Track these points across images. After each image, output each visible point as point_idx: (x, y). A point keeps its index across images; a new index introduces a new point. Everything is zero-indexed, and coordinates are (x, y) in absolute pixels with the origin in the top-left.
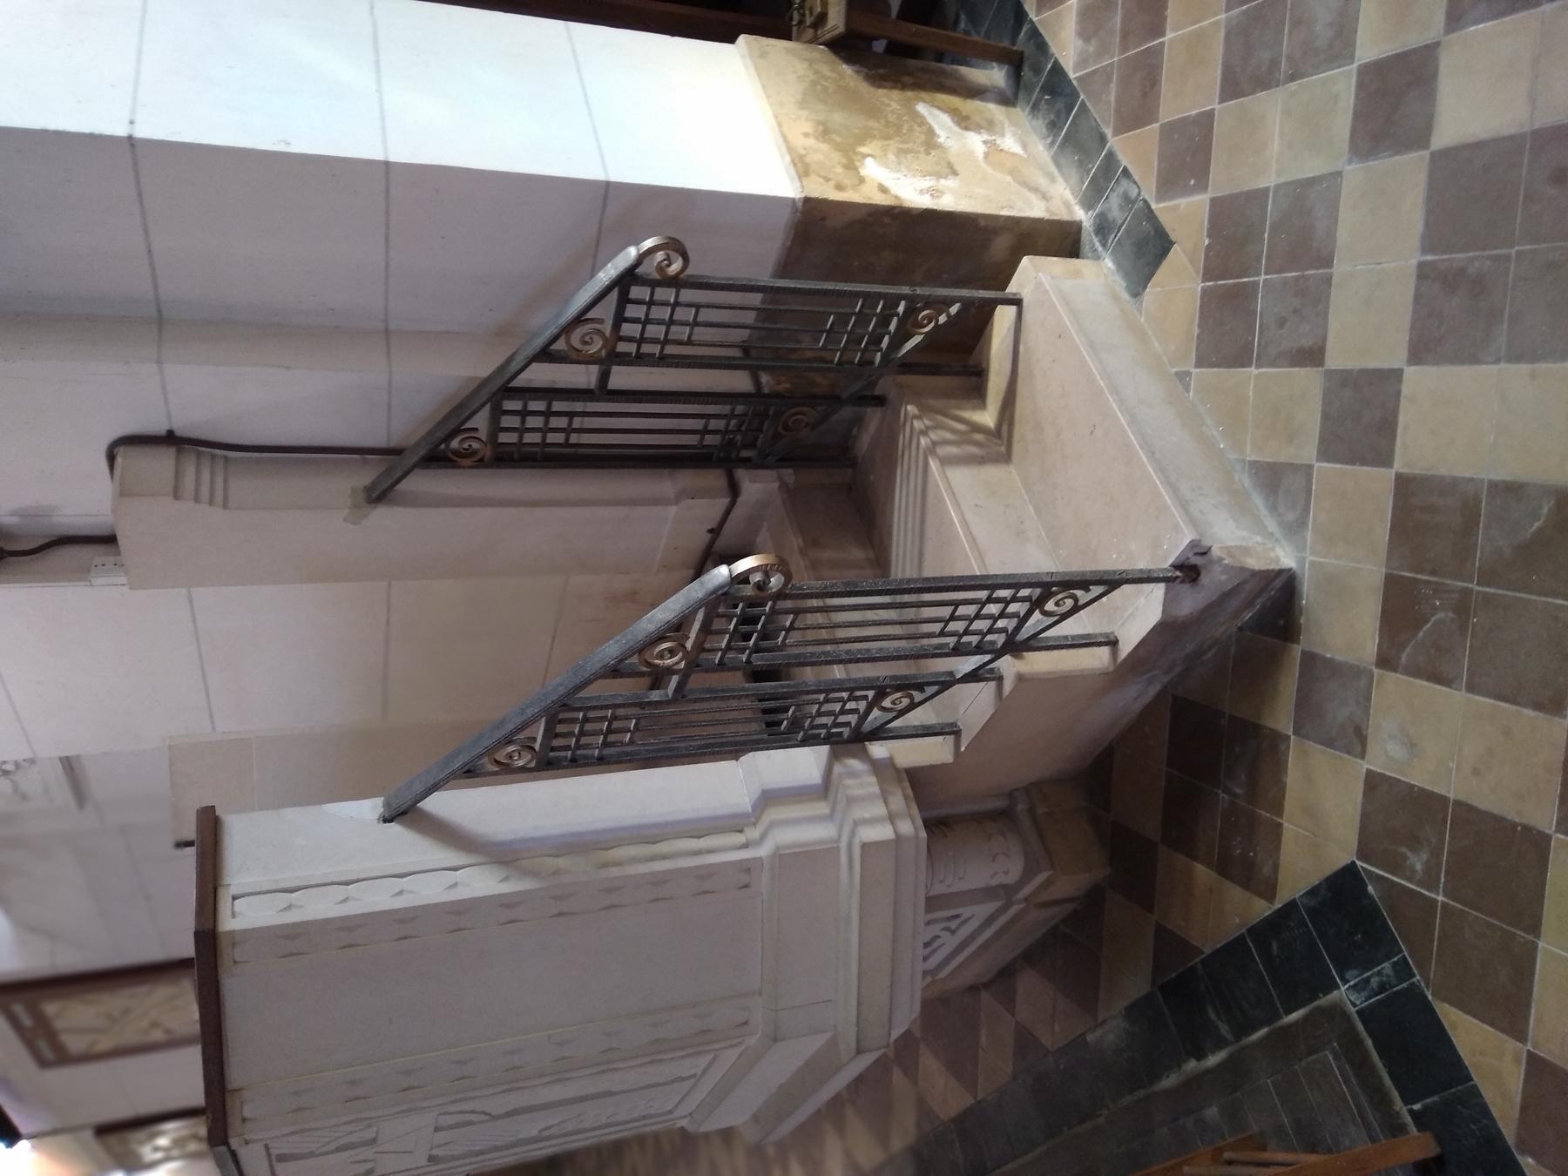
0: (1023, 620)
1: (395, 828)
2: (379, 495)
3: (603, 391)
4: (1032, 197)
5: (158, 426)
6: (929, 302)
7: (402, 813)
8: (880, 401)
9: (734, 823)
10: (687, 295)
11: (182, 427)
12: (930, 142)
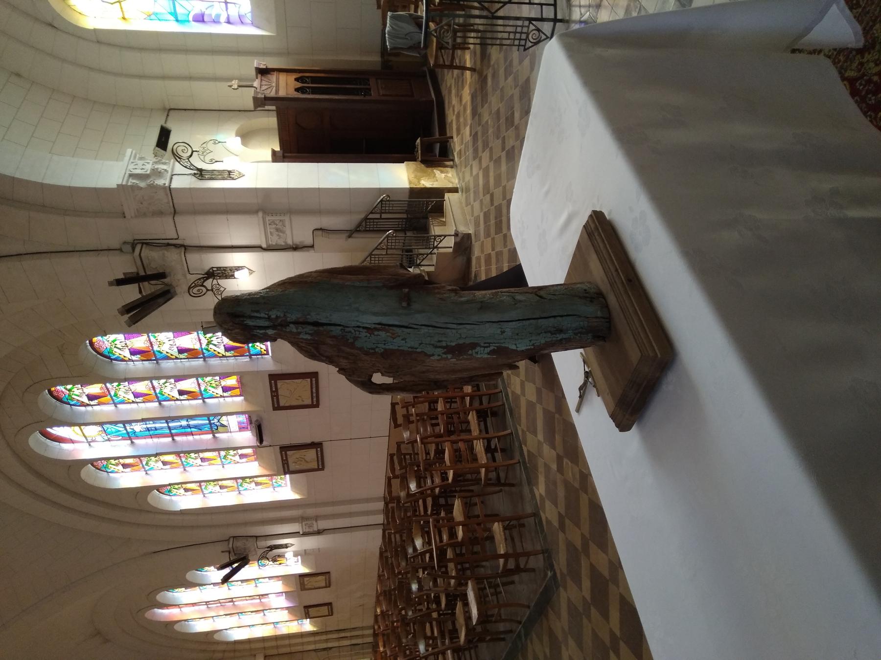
2: (350, 237)
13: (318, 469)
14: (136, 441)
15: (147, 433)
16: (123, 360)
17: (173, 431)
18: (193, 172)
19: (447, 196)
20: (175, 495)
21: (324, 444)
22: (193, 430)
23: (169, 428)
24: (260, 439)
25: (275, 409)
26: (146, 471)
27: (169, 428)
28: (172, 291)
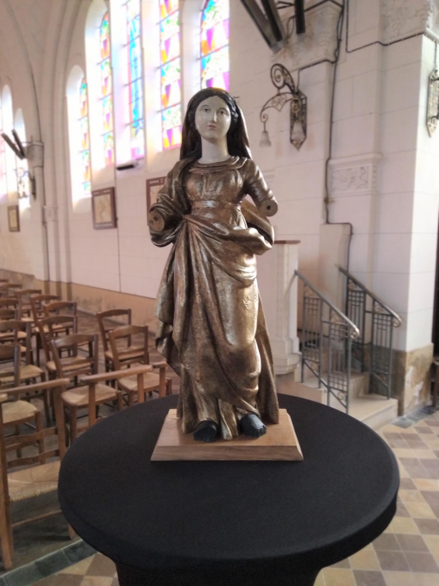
0: (337, 389)
3: (365, 311)
5: (354, 231)
6: (387, 380)
7: (296, 273)
9: (288, 335)
10: (389, 329)
11: (353, 236)
12: (417, 383)
14: (126, 49)
15: (133, 59)
16: (202, 22)
19: (394, 402)
20: (81, 93)
21: (114, 231)
23: (136, 81)
24: (121, 168)
25: (148, 181)
27: (136, 81)
28: (280, 44)
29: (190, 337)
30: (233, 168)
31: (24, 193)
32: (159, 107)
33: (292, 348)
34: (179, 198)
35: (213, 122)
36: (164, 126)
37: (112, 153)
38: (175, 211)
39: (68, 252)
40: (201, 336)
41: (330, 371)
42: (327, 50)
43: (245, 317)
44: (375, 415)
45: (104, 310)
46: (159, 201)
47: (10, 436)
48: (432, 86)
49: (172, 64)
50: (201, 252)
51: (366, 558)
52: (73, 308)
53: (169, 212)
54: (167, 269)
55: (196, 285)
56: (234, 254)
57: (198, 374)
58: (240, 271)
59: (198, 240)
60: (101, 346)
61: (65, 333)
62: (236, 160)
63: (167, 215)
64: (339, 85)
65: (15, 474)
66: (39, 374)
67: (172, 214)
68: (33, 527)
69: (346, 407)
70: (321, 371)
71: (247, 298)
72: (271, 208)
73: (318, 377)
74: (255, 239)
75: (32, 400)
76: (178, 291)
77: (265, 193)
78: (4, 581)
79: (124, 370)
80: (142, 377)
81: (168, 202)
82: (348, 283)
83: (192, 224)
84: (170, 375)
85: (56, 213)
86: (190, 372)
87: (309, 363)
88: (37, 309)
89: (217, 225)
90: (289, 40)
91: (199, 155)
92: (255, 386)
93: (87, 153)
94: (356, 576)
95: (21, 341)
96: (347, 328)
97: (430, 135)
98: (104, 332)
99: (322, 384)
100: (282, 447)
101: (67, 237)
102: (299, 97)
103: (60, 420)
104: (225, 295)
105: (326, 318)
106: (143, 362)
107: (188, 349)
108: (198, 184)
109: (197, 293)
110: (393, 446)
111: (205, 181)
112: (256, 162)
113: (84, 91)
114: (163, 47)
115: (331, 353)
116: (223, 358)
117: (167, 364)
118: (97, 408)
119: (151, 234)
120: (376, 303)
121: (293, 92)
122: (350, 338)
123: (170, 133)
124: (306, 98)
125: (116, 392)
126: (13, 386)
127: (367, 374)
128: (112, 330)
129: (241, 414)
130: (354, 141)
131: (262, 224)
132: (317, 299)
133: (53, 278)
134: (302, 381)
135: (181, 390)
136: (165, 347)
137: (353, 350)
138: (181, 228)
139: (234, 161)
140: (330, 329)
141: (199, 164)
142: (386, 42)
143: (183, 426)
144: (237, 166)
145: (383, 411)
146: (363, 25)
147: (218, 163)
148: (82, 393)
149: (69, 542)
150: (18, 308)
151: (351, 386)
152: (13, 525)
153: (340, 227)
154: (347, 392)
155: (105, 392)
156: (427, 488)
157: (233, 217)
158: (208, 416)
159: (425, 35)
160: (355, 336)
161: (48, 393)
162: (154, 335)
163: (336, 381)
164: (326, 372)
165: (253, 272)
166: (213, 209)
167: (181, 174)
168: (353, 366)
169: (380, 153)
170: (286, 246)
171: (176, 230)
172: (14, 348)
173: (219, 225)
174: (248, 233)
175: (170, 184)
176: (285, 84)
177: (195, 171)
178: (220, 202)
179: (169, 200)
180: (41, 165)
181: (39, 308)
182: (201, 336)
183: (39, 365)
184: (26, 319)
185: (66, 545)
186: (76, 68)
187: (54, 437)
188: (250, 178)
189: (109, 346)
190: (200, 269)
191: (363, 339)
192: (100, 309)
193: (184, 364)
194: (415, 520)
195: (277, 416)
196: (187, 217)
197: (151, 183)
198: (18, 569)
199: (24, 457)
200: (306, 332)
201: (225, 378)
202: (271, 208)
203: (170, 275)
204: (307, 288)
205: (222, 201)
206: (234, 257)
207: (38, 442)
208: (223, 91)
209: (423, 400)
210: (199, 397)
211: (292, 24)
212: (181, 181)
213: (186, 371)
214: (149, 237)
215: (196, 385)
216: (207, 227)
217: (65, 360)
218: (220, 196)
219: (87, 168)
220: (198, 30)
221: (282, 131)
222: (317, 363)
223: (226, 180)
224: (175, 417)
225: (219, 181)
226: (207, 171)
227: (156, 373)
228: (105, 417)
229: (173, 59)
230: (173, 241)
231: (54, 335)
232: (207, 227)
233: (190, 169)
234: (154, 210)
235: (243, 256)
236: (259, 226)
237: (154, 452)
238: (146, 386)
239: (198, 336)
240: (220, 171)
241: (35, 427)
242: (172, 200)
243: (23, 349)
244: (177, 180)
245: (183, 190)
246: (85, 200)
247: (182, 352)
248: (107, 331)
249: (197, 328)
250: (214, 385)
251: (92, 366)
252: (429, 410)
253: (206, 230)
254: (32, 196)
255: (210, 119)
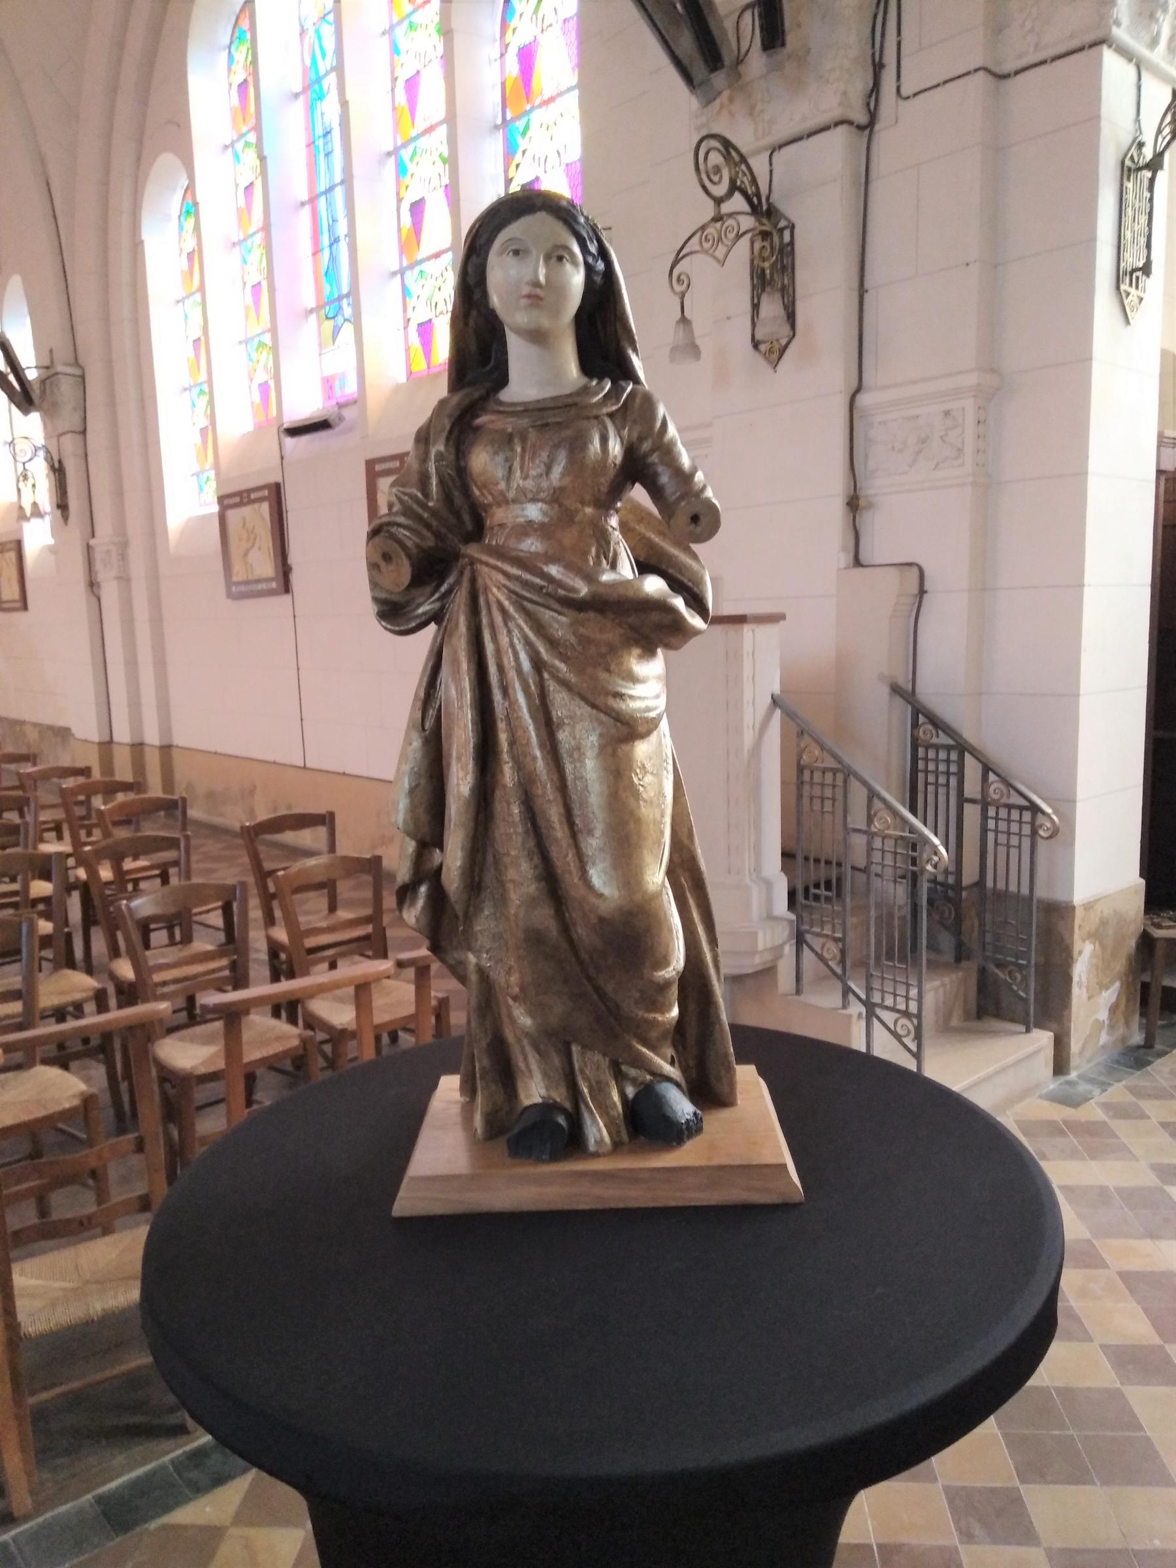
0: (893, 1009)
1: (769, 700)
2: (896, 690)
3: (962, 800)
4: (1080, 1045)
5: (927, 587)
6: (1025, 979)
7: (775, 702)
8: (958, 959)
9: (758, 869)
10: (1026, 843)
12: (1104, 987)
13: (229, 582)
15: (319, 131)
17: (322, 200)
18: (1148, 137)
19: (1043, 1038)
20: (181, 228)
22: (326, 254)
23: (331, 189)
24: (295, 431)
25: (370, 464)
26: (232, 144)
27: (331, 189)
28: (719, 79)
29: (489, 877)
30: (595, 412)
31: (35, 504)
32: (393, 261)
33: (769, 902)
34: (447, 498)
35: (536, 284)
36: (410, 314)
37: (270, 391)
38: (437, 535)
39: (161, 664)
40: (519, 876)
41: (872, 962)
42: (845, 93)
43: (638, 821)
44: (993, 1072)
45: (263, 815)
46: (395, 509)
47: (19, 1161)
48: (1129, 185)
49: (423, 142)
50: (512, 645)
51: (980, 1454)
52: (179, 813)
53: (423, 538)
54: (422, 694)
55: (503, 737)
56: (604, 650)
57: (514, 979)
58: (620, 696)
59: (503, 611)
60: (256, 914)
61: (158, 881)
62: (603, 389)
63: (418, 546)
64: (879, 189)
65: (31, 1264)
66: (91, 993)
67: (430, 542)
68: (82, 1404)
69: (917, 1056)
70: (848, 963)
71: (644, 767)
72: (702, 521)
73: (842, 978)
74: (661, 606)
75: (74, 1065)
76: (454, 754)
77: (685, 478)
78: (13, 1548)
79: (320, 975)
80: (369, 993)
81: (420, 511)
82: (915, 725)
83: (485, 569)
84: (442, 986)
85: (123, 557)
86: (493, 975)
87: (817, 943)
88: (82, 818)
89: (554, 570)
90: (742, 68)
91: (502, 380)
92: (670, 1009)
93: (202, 392)
94: (951, 1502)
95: (41, 907)
96: (915, 844)
97: (1128, 322)
98: (263, 875)
99: (851, 997)
100: (746, 1169)
101: (157, 621)
102: (775, 226)
103: (150, 1112)
104: (582, 762)
105: (857, 819)
106: (370, 953)
107: (486, 913)
108: (500, 459)
109: (505, 756)
110: (1044, 1157)
111: (519, 449)
112: (657, 395)
113: (190, 223)
114: (401, 97)
115: (873, 913)
116: (581, 931)
117: (434, 958)
118: (250, 1080)
119: (376, 600)
120: (992, 777)
121: (755, 210)
122: (923, 870)
123: (425, 330)
124: (792, 227)
125: (300, 1035)
126: (20, 1027)
127: (970, 968)
128: (284, 869)
129: (634, 1081)
130: (924, 345)
131: (680, 567)
132: (835, 771)
133: (123, 734)
134: (798, 992)
135: (469, 1022)
136: (423, 908)
137: (931, 902)
138: (458, 582)
139: (597, 393)
140: (870, 849)
141: (501, 403)
142: (1009, 67)
143: (478, 1121)
144: (606, 405)
145: (1016, 1064)
146: (940, 33)
147: (554, 399)
148: (207, 1040)
149: (185, 1438)
150: (29, 818)
151: (929, 1000)
152: (31, 1400)
153: (893, 574)
154: (919, 1016)
155: (268, 1036)
156: (1134, 1265)
157: (599, 546)
158: (543, 1092)
159: (1110, 46)
160: (935, 866)
161: (117, 1044)
162: (392, 876)
163: (889, 988)
164: (863, 963)
165: (657, 697)
166: (542, 525)
167: (451, 432)
168: (932, 947)
169: (994, 371)
170: (747, 630)
171: (443, 589)
172: (20, 924)
173: (561, 569)
174: (639, 589)
175: (424, 459)
176: (733, 188)
177: (492, 422)
178: (560, 505)
179: (424, 506)
180: (81, 429)
181: (88, 817)
182: (519, 876)
183: (90, 971)
184: (50, 847)
185: (177, 1448)
186: (167, 161)
187: (136, 1160)
188: (641, 439)
189: (278, 914)
190: (510, 691)
191: (959, 872)
192: (251, 812)
193: (477, 953)
194: (1105, 1348)
195: (732, 1084)
196: (472, 550)
197: (378, 468)
198: (48, 1515)
199: (56, 1215)
200: (807, 859)
201: (589, 988)
202: (702, 518)
203: (432, 713)
204: (806, 740)
205: (567, 503)
206: (603, 656)
207: (93, 1174)
208: (561, 197)
209: (1121, 1030)
210: (519, 1041)
211: (750, 24)
212: (453, 450)
213: (480, 970)
214: (371, 609)
215: (509, 1008)
216: (527, 576)
217: (161, 952)
218: (562, 489)
219: (203, 431)
220: (496, 51)
221: (729, 318)
222: (836, 940)
223: (577, 445)
224: (456, 1096)
225: (557, 446)
226: (524, 422)
227: (408, 982)
228: (268, 1103)
229: (430, 130)
230: (437, 617)
231: (130, 887)
232: (527, 576)
233: (478, 416)
234: (382, 534)
235: (630, 654)
236: (671, 571)
237: (401, 1194)
238: (380, 1017)
239: (511, 874)
240: (559, 419)
241: (83, 1136)
242: (431, 504)
243: (45, 927)
244: (442, 448)
245: (459, 476)
246: (205, 518)
247: (468, 919)
248: (272, 873)
249: (508, 854)
250: (558, 1008)
251: (233, 966)
252: (1137, 1058)
253: (526, 584)
254: (59, 512)
255: (528, 277)
